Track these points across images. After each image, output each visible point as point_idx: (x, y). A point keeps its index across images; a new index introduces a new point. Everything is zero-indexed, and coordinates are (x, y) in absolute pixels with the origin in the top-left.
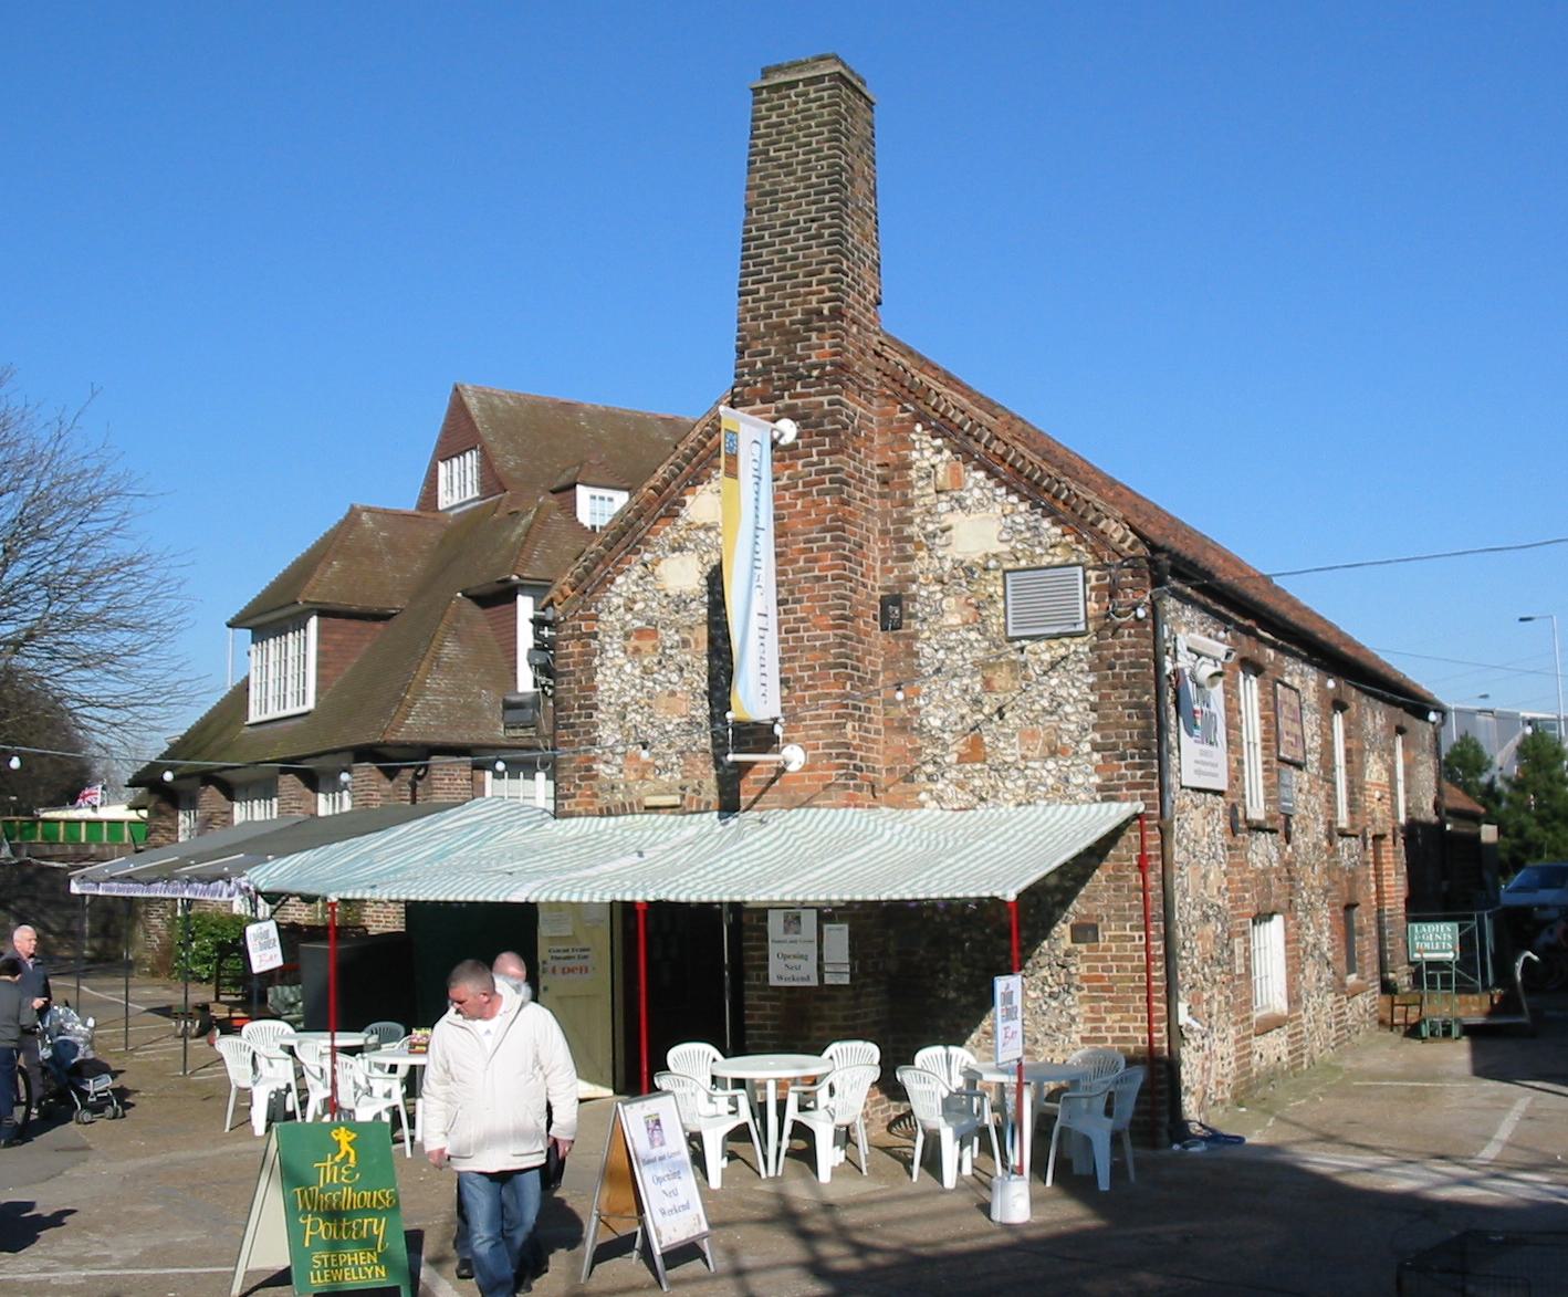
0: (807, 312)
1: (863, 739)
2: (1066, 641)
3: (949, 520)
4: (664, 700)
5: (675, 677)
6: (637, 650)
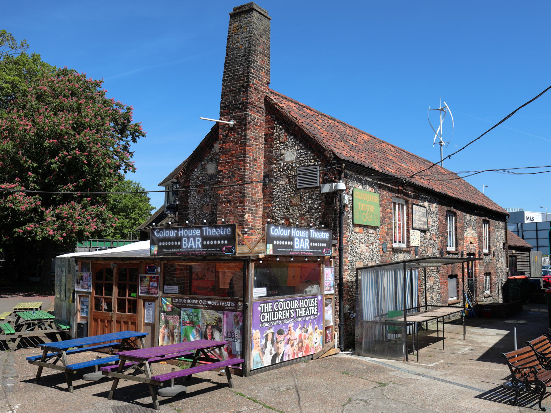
0: (240, 86)
1: (252, 219)
2: (313, 189)
3: (283, 151)
4: (205, 206)
5: (208, 200)
6: (199, 191)
